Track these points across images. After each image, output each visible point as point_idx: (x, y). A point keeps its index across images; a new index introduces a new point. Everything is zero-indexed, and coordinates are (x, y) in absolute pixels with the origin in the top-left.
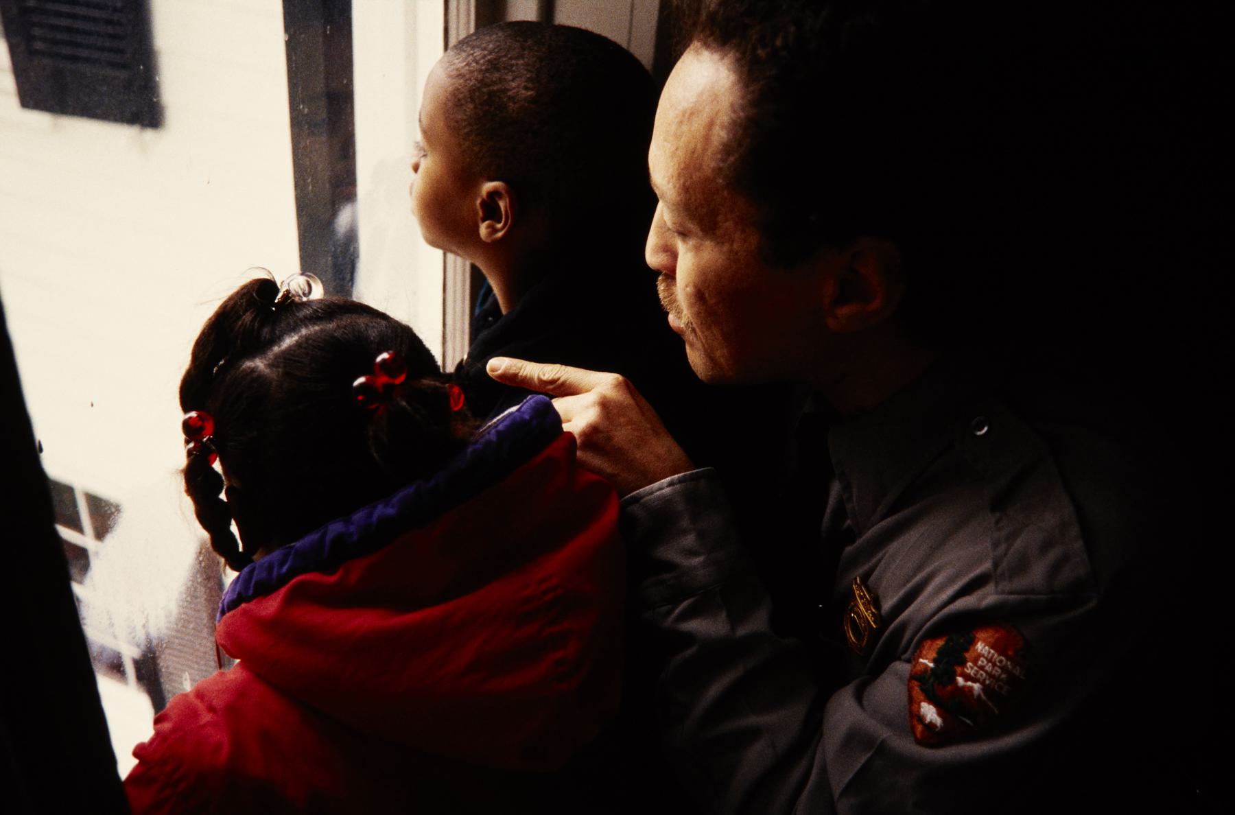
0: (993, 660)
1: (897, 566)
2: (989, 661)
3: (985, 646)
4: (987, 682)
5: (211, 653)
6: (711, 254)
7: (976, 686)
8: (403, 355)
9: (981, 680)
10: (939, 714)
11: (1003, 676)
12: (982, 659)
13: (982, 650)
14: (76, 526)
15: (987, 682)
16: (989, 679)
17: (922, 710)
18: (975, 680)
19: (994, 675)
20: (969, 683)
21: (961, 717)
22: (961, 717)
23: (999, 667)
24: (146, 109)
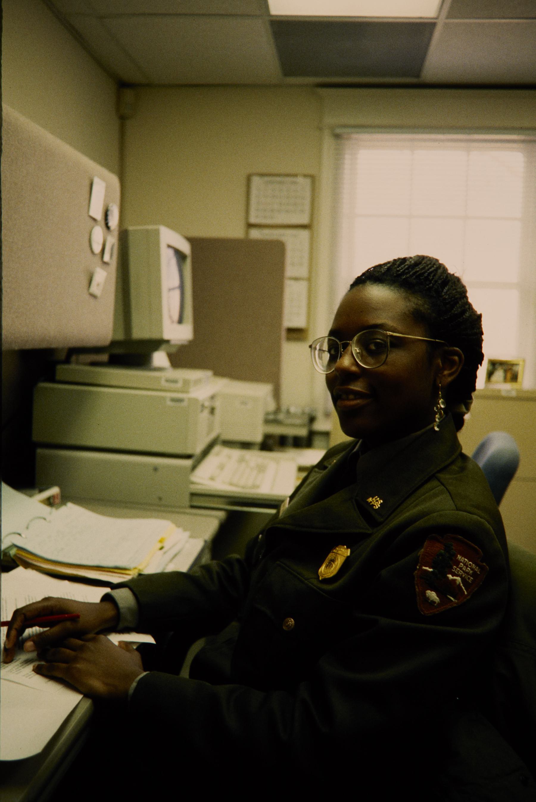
0: (466, 564)
1: (469, 515)
2: (465, 564)
3: (462, 558)
4: (464, 576)
5: (130, 447)
6: (117, 644)
7: (459, 579)
8: (434, 315)
9: (460, 575)
10: (438, 596)
11: (471, 572)
12: (461, 564)
13: (460, 559)
14: (454, 570)
15: (464, 576)
16: (464, 574)
17: (427, 594)
18: (457, 576)
19: (467, 572)
20: (455, 578)
21: (449, 596)
22: (449, 596)
23: (469, 568)
24: (258, 306)
